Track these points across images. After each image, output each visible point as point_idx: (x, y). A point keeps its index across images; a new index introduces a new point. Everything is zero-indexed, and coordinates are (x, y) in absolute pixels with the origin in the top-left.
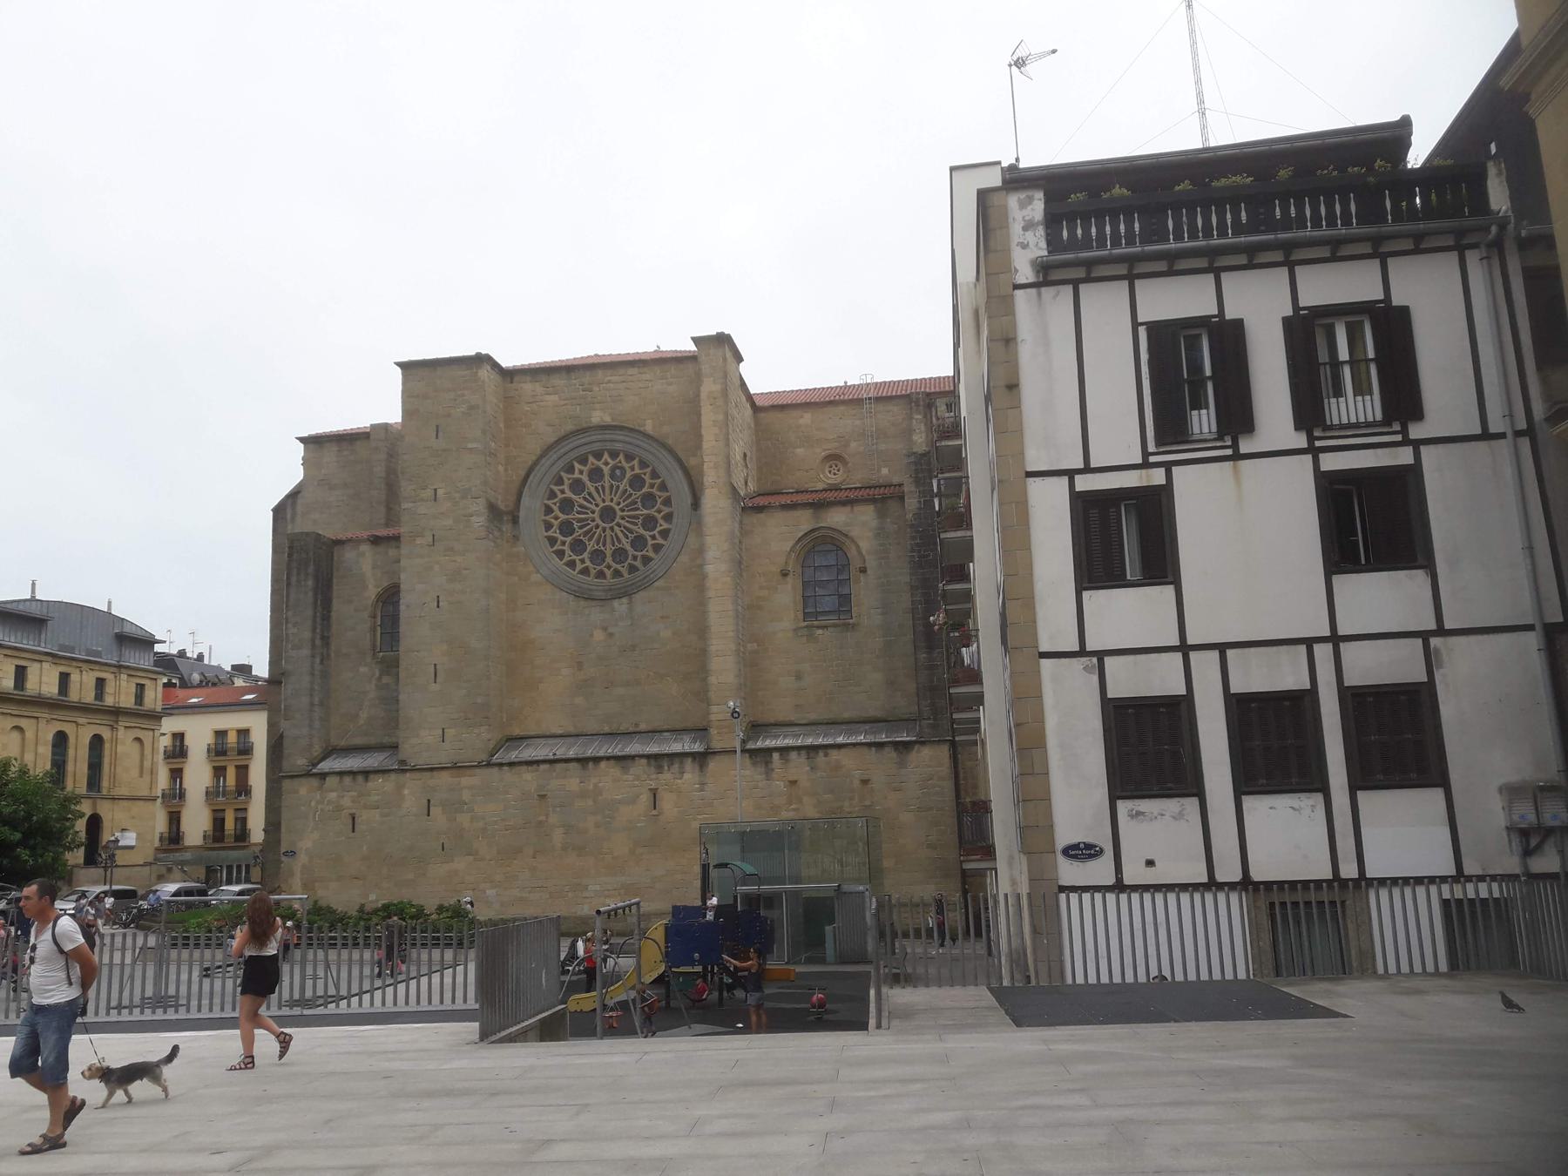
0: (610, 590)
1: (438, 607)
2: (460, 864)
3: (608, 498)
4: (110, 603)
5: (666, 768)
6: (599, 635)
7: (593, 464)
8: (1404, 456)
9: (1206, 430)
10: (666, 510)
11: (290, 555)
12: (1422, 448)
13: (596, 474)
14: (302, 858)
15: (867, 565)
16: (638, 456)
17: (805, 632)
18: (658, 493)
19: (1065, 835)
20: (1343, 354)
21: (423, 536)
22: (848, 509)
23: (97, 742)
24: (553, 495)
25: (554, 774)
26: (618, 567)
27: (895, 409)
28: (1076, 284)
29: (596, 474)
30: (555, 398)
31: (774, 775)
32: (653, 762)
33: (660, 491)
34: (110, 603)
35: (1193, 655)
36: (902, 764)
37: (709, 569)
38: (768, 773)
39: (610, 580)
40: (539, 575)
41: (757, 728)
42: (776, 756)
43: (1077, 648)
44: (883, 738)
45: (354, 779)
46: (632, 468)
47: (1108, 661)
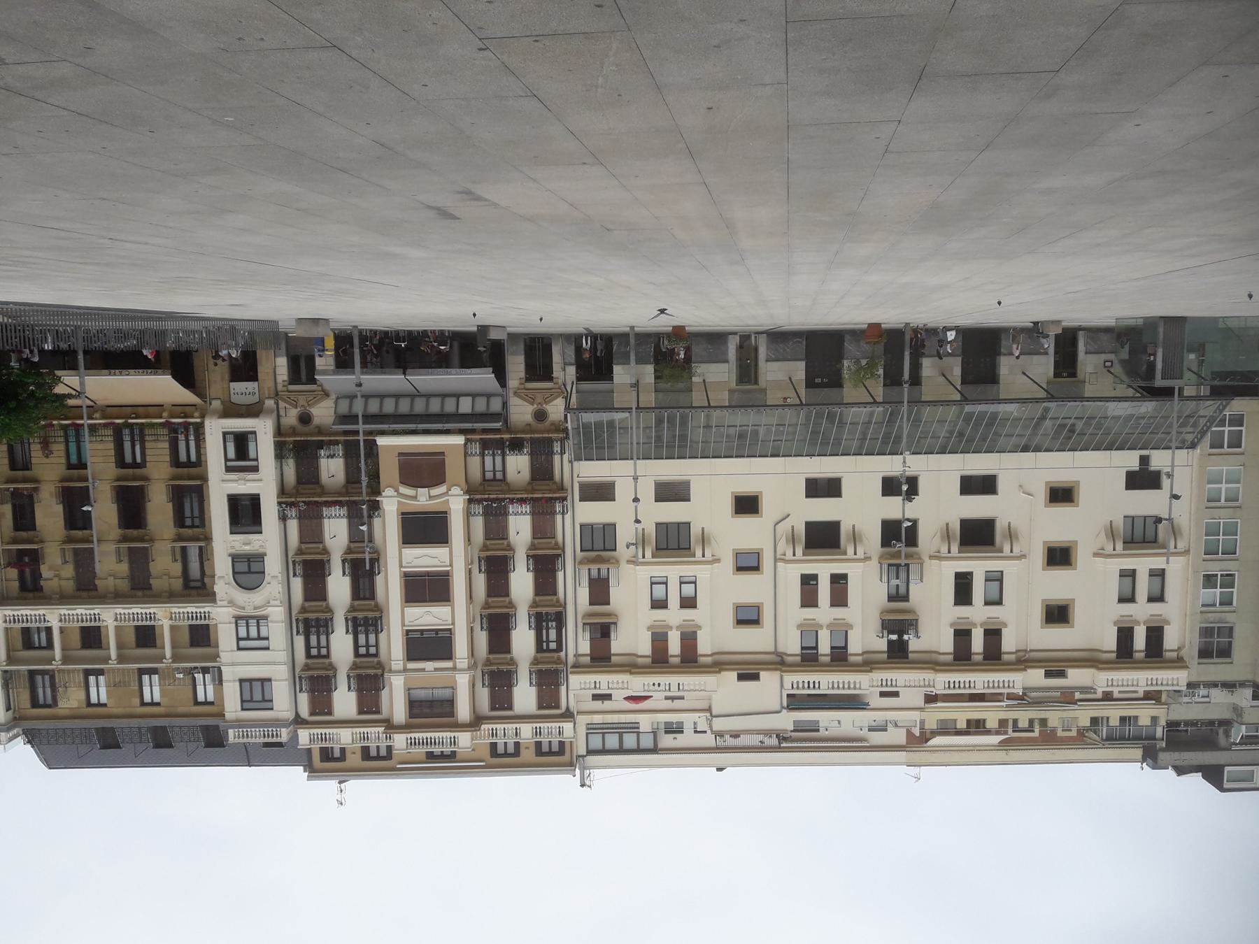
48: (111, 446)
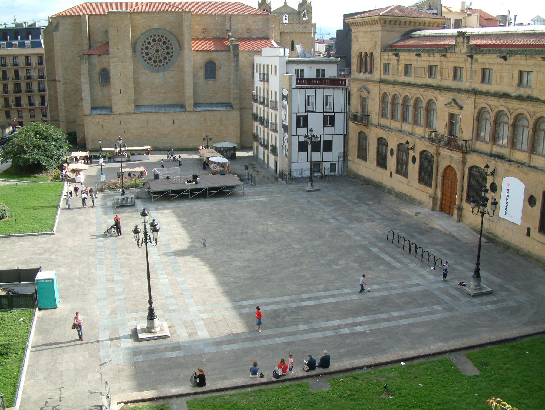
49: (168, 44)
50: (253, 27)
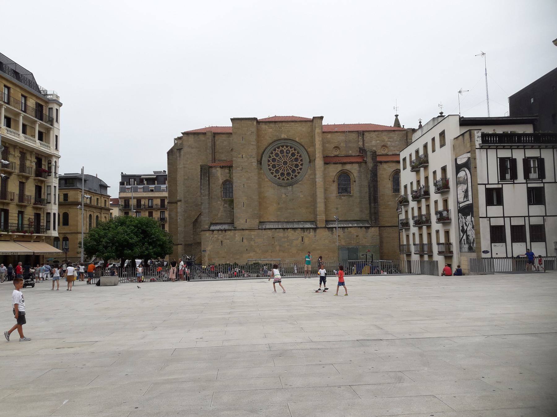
0: (287, 184)
1: (244, 187)
2: (252, 254)
3: (285, 158)
4: (97, 175)
5: (306, 231)
6: (284, 196)
7: (281, 149)
8: (542, 185)
9: (508, 178)
10: (301, 163)
11: (201, 171)
12: (545, 184)
13: (282, 152)
14: (208, 252)
15: (356, 180)
16: (284, 145)
17: (339, 197)
18: (299, 158)
19: (483, 249)
20: (532, 166)
21: (239, 167)
22: (351, 165)
23: (97, 216)
24: (270, 157)
25: (276, 232)
26: (288, 177)
27: (354, 135)
28: (487, 149)
29: (282, 152)
30: (271, 130)
31: (334, 234)
32: (302, 230)
33: (299, 157)
34: (97, 175)
35: (505, 218)
36: (367, 232)
37: (317, 180)
38: (332, 233)
39: (286, 181)
40: (267, 179)
41: (327, 221)
42: (334, 229)
43: (486, 216)
44: (361, 225)
45: (222, 232)
46: (292, 151)
47: (491, 219)
48: (10, 221)
49: (297, 156)
50: (337, 244)
